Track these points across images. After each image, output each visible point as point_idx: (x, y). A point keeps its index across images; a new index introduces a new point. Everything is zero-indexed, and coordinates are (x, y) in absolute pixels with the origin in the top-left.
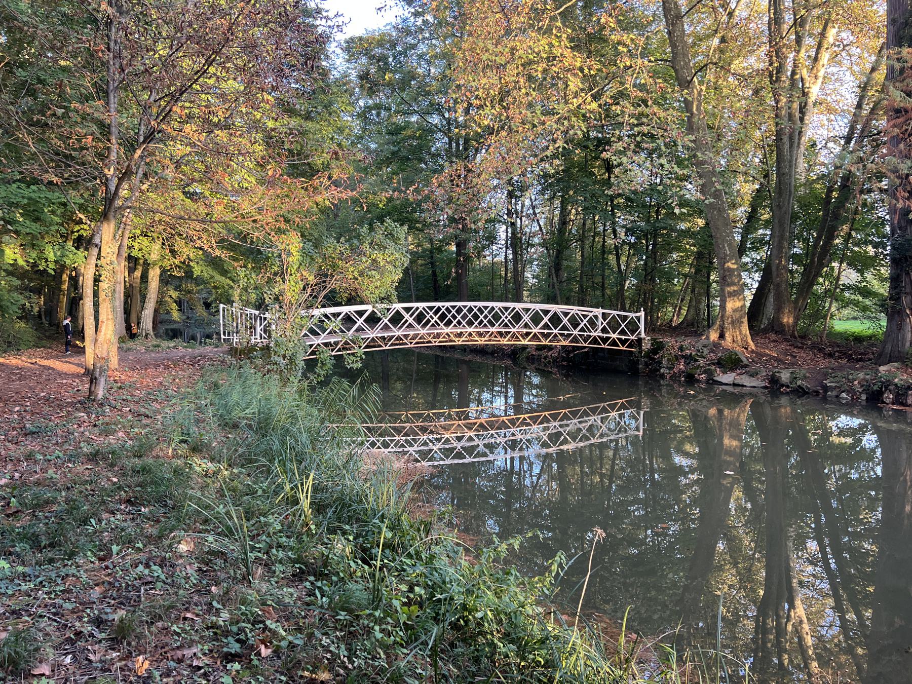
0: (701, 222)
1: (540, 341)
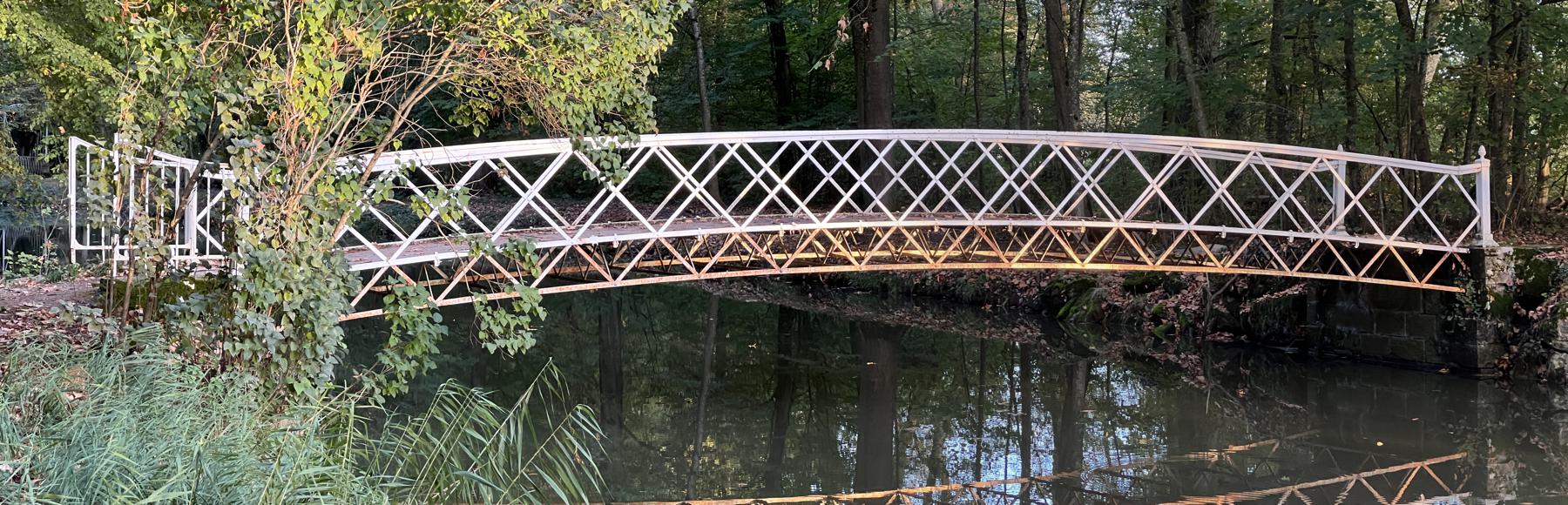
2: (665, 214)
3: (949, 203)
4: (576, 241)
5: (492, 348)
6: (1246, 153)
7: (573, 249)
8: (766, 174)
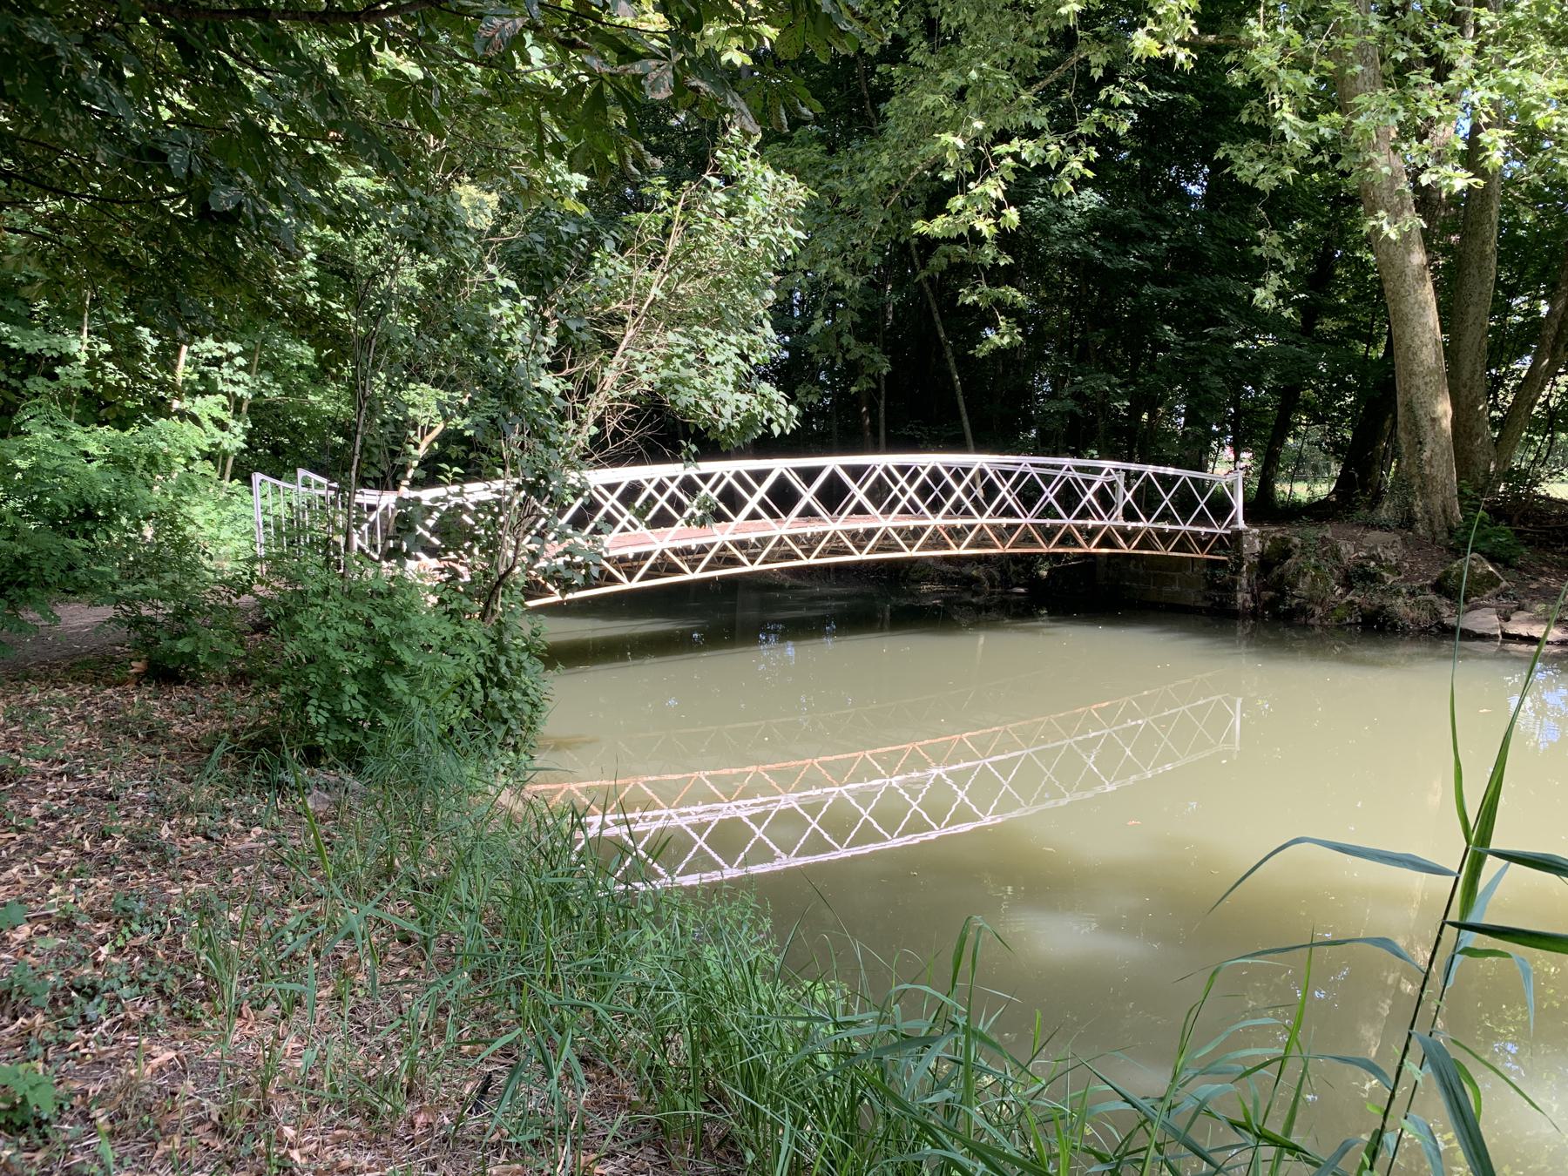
0: (1481, 182)
1: (1077, 545)
3: (808, 506)
5: (301, 473)
8: (673, 496)
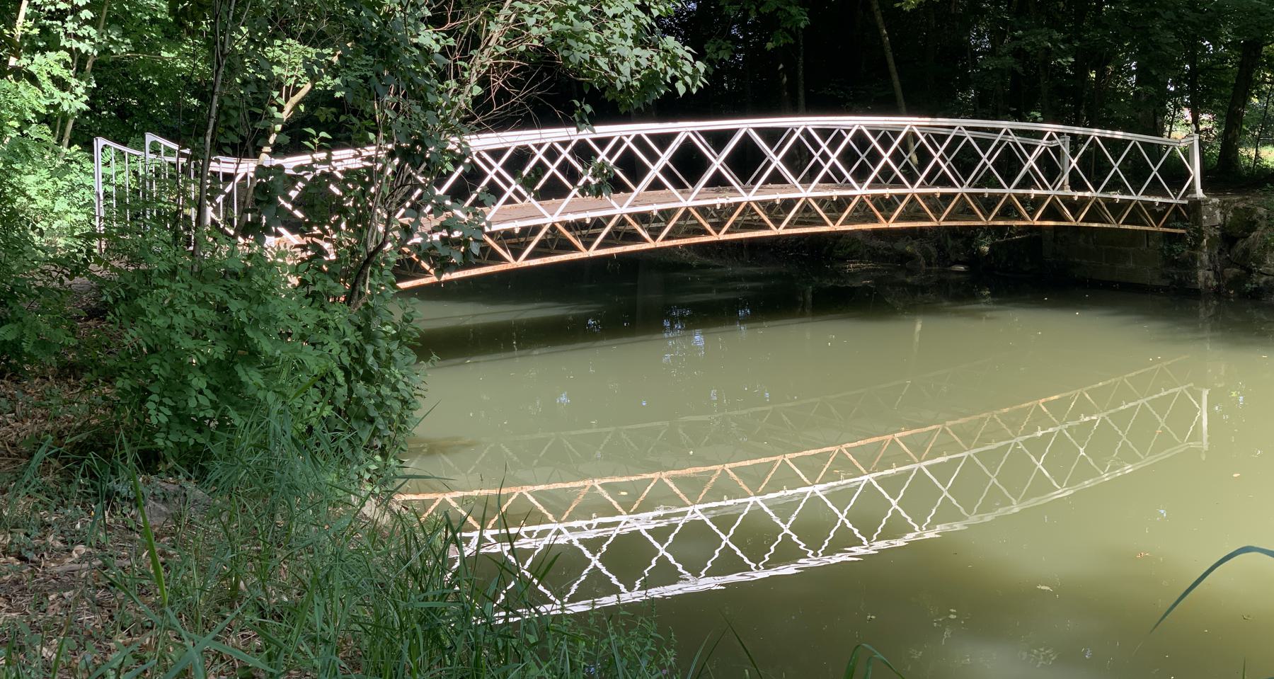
2: (754, 182)
4: (556, 218)
6: (953, 127)
7: (748, 205)
